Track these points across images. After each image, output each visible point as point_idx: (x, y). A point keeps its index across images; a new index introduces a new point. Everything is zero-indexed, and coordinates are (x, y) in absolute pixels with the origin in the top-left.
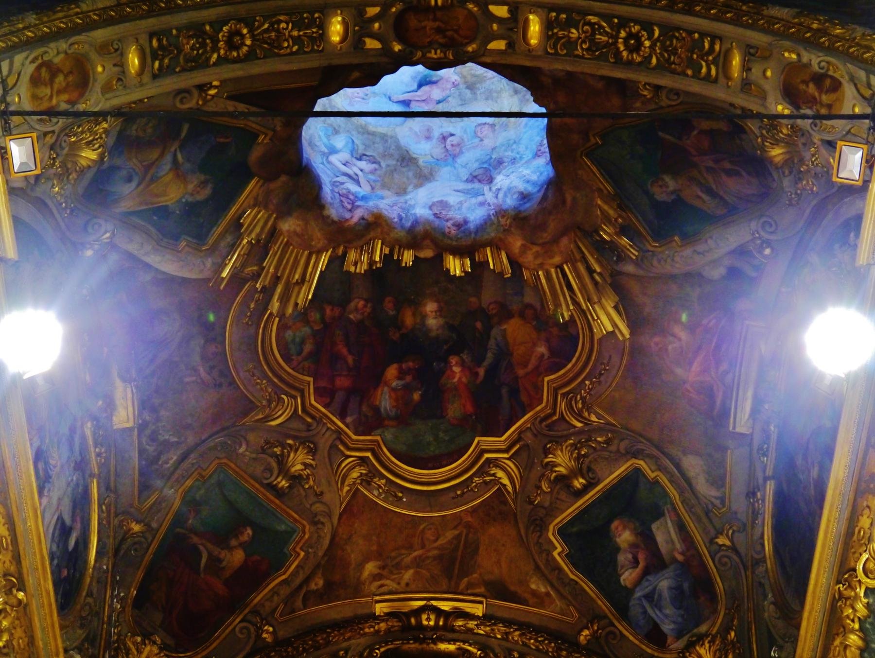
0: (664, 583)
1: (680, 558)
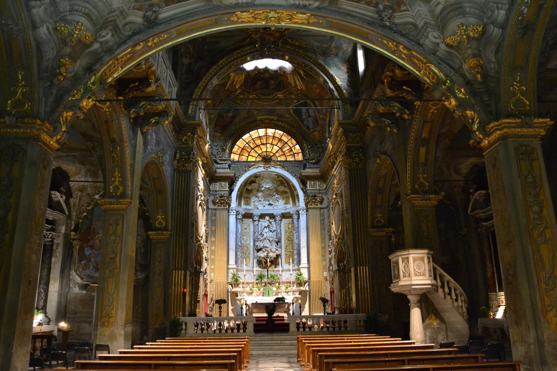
0: (310, 119)
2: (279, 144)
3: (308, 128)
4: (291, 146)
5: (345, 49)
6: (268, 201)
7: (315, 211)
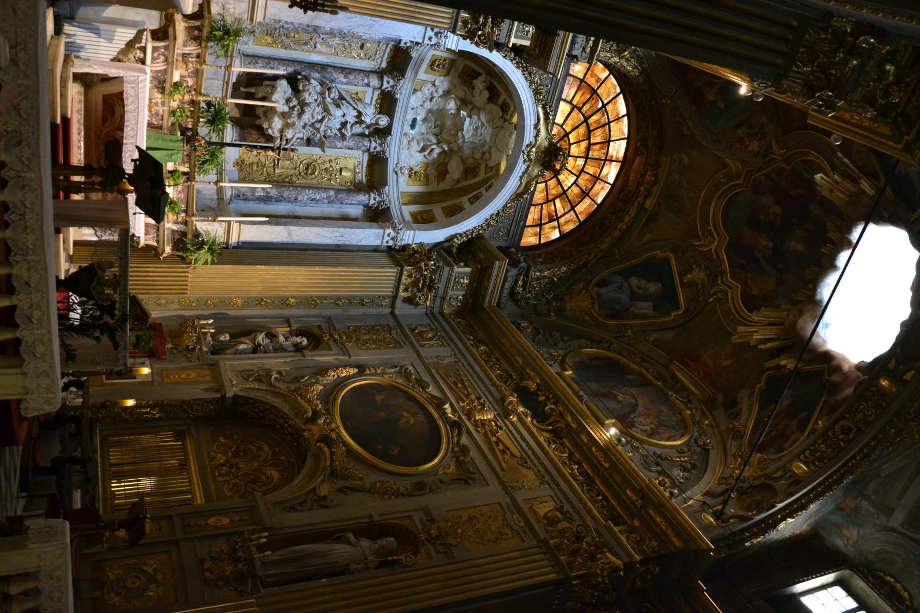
0: (624, 298)
1: (632, 309)
2: (575, 190)
3: (602, 283)
4: (562, 220)
5: (845, 532)
6: (425, 120)
7: (392, 282)
